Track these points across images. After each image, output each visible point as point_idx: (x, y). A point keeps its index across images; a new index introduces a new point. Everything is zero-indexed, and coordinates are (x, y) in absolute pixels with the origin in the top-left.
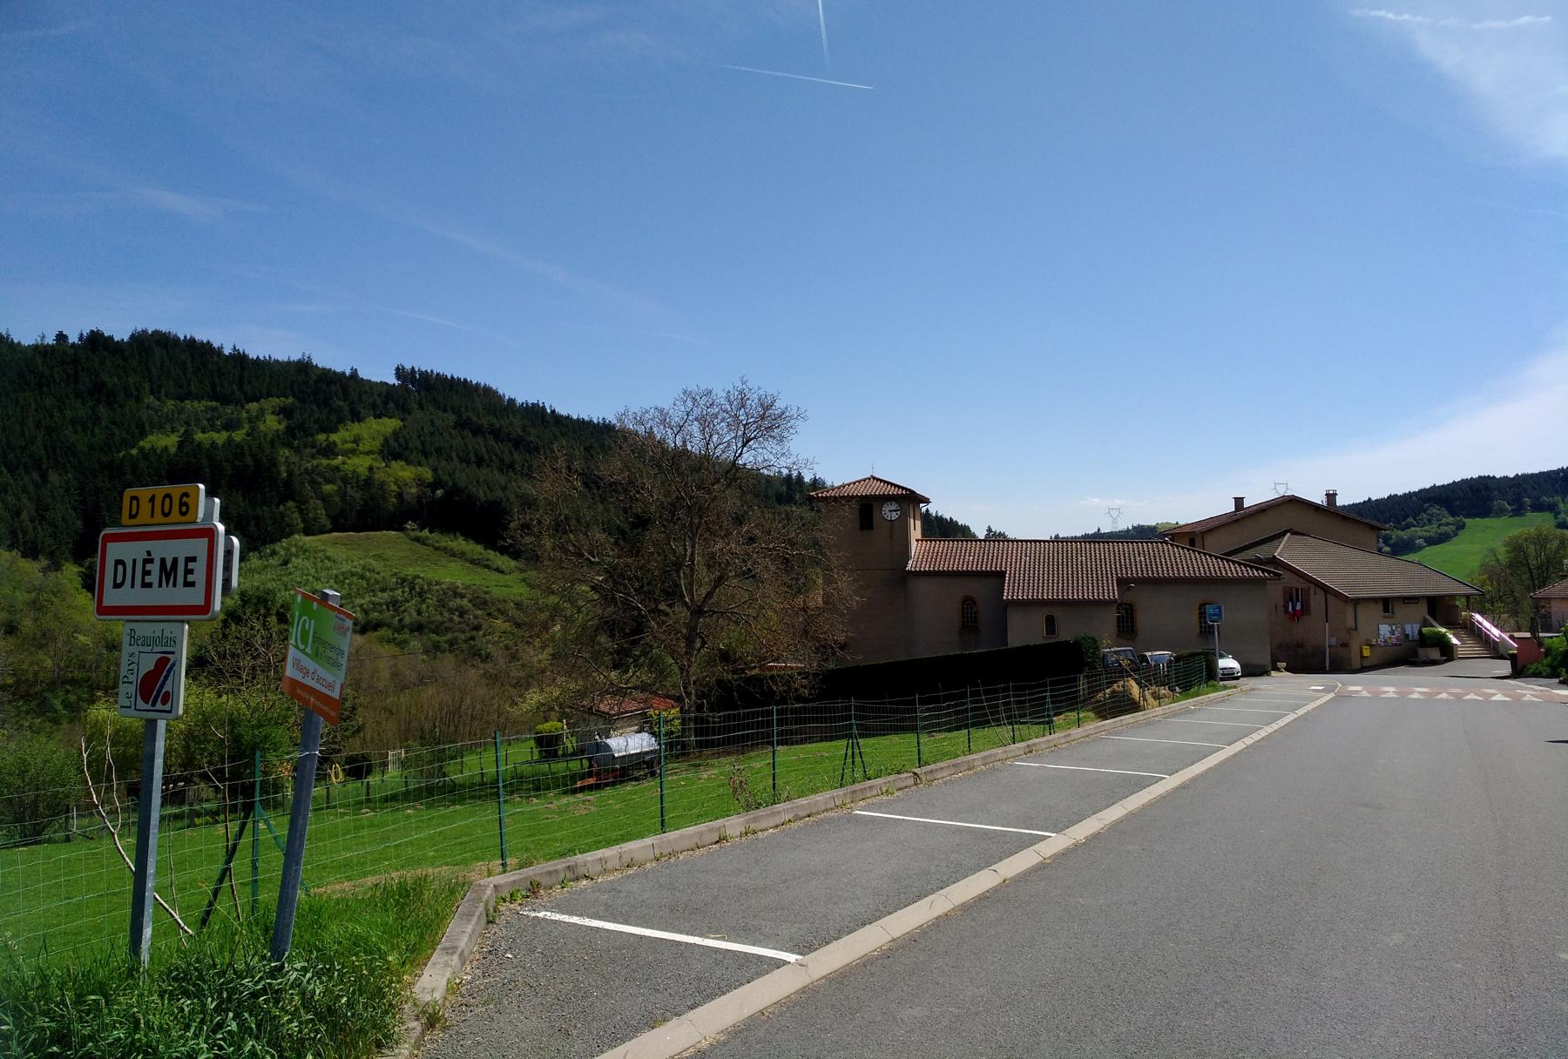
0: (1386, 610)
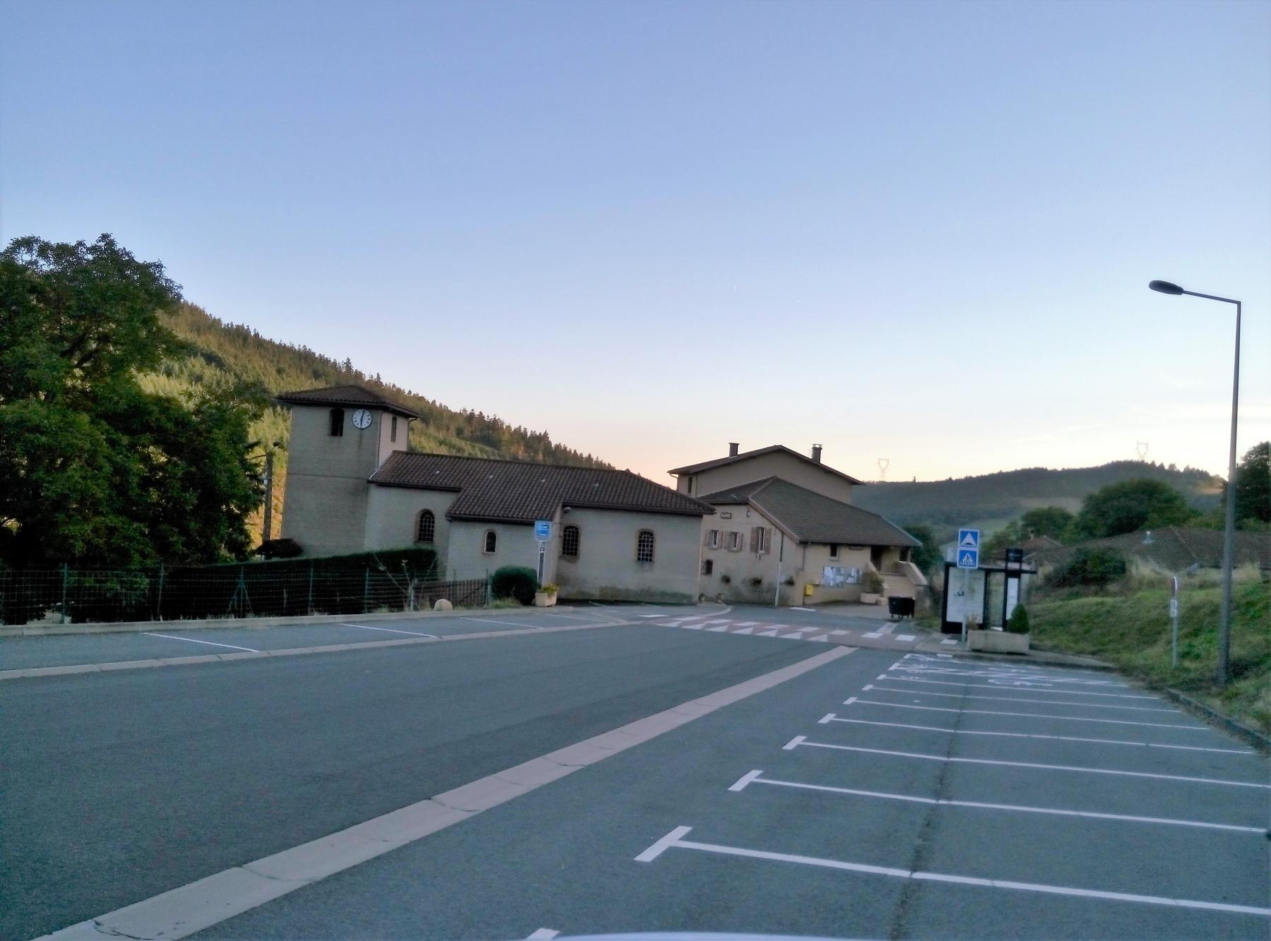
0: (834, 553)
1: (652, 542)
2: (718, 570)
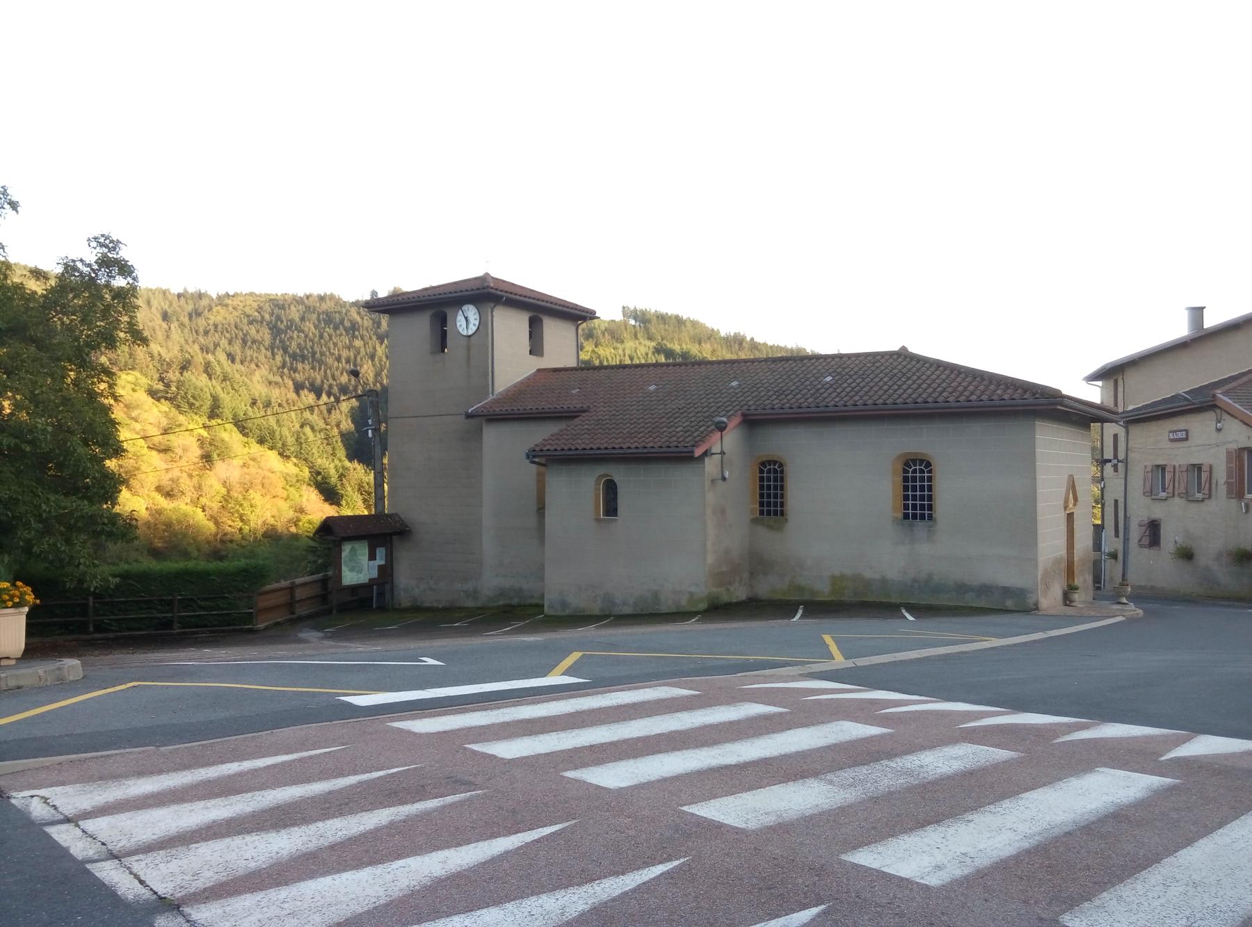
1: (930, 479)
2: (1171, 537)
